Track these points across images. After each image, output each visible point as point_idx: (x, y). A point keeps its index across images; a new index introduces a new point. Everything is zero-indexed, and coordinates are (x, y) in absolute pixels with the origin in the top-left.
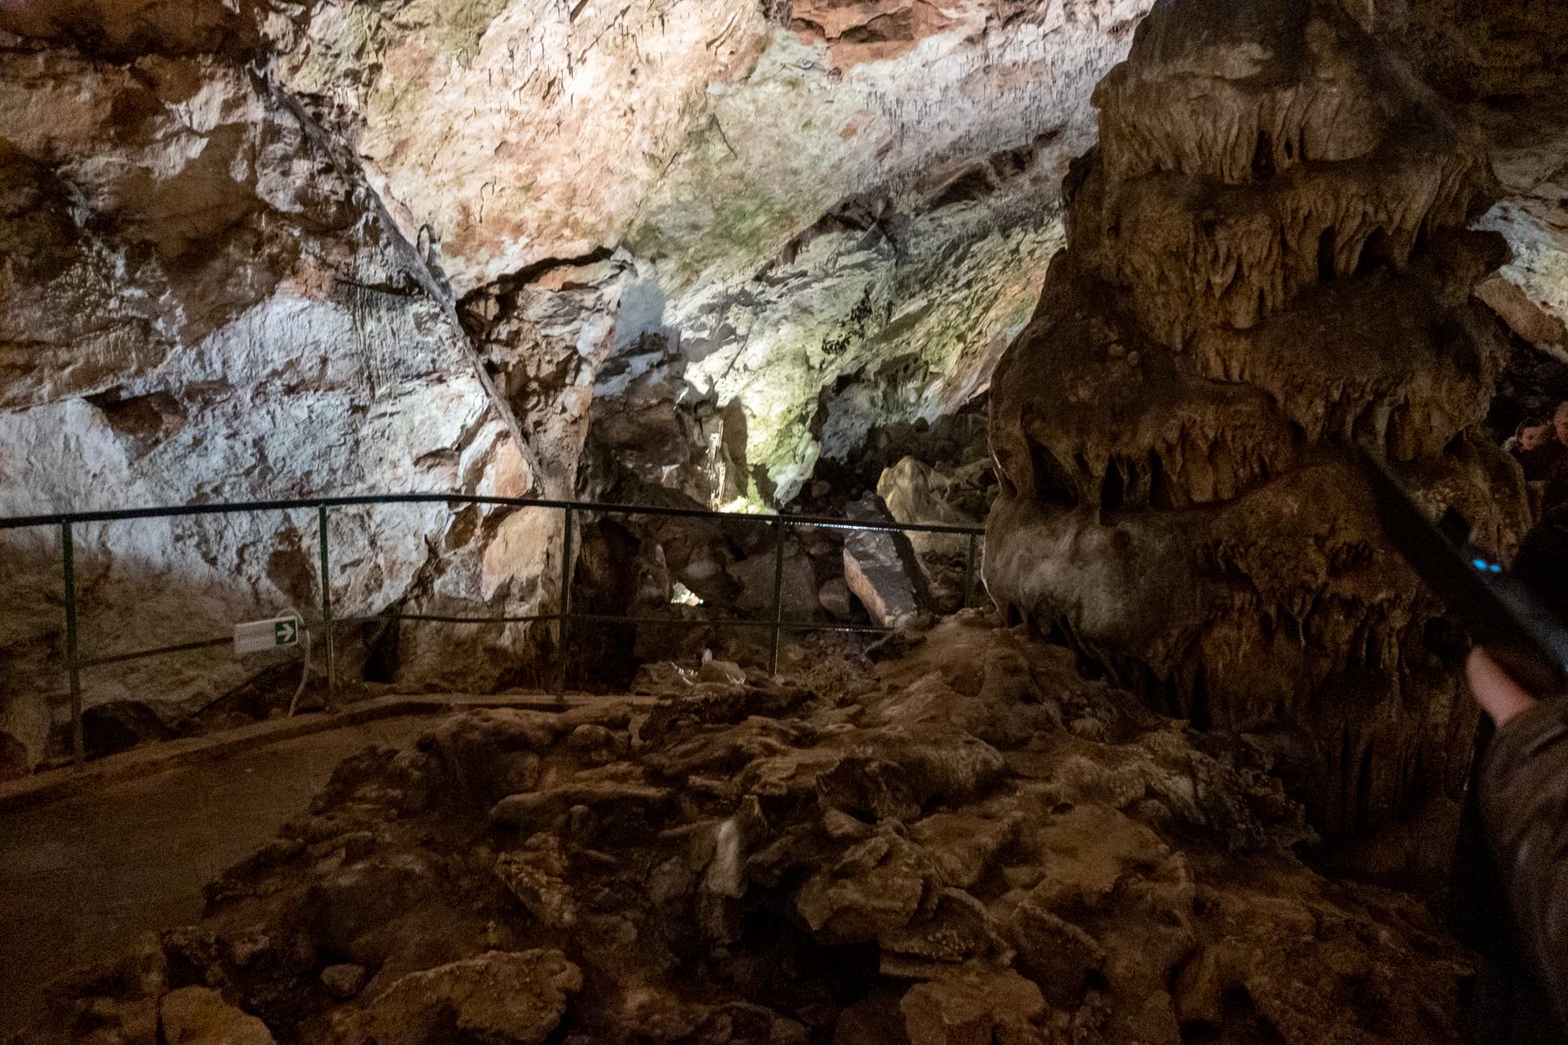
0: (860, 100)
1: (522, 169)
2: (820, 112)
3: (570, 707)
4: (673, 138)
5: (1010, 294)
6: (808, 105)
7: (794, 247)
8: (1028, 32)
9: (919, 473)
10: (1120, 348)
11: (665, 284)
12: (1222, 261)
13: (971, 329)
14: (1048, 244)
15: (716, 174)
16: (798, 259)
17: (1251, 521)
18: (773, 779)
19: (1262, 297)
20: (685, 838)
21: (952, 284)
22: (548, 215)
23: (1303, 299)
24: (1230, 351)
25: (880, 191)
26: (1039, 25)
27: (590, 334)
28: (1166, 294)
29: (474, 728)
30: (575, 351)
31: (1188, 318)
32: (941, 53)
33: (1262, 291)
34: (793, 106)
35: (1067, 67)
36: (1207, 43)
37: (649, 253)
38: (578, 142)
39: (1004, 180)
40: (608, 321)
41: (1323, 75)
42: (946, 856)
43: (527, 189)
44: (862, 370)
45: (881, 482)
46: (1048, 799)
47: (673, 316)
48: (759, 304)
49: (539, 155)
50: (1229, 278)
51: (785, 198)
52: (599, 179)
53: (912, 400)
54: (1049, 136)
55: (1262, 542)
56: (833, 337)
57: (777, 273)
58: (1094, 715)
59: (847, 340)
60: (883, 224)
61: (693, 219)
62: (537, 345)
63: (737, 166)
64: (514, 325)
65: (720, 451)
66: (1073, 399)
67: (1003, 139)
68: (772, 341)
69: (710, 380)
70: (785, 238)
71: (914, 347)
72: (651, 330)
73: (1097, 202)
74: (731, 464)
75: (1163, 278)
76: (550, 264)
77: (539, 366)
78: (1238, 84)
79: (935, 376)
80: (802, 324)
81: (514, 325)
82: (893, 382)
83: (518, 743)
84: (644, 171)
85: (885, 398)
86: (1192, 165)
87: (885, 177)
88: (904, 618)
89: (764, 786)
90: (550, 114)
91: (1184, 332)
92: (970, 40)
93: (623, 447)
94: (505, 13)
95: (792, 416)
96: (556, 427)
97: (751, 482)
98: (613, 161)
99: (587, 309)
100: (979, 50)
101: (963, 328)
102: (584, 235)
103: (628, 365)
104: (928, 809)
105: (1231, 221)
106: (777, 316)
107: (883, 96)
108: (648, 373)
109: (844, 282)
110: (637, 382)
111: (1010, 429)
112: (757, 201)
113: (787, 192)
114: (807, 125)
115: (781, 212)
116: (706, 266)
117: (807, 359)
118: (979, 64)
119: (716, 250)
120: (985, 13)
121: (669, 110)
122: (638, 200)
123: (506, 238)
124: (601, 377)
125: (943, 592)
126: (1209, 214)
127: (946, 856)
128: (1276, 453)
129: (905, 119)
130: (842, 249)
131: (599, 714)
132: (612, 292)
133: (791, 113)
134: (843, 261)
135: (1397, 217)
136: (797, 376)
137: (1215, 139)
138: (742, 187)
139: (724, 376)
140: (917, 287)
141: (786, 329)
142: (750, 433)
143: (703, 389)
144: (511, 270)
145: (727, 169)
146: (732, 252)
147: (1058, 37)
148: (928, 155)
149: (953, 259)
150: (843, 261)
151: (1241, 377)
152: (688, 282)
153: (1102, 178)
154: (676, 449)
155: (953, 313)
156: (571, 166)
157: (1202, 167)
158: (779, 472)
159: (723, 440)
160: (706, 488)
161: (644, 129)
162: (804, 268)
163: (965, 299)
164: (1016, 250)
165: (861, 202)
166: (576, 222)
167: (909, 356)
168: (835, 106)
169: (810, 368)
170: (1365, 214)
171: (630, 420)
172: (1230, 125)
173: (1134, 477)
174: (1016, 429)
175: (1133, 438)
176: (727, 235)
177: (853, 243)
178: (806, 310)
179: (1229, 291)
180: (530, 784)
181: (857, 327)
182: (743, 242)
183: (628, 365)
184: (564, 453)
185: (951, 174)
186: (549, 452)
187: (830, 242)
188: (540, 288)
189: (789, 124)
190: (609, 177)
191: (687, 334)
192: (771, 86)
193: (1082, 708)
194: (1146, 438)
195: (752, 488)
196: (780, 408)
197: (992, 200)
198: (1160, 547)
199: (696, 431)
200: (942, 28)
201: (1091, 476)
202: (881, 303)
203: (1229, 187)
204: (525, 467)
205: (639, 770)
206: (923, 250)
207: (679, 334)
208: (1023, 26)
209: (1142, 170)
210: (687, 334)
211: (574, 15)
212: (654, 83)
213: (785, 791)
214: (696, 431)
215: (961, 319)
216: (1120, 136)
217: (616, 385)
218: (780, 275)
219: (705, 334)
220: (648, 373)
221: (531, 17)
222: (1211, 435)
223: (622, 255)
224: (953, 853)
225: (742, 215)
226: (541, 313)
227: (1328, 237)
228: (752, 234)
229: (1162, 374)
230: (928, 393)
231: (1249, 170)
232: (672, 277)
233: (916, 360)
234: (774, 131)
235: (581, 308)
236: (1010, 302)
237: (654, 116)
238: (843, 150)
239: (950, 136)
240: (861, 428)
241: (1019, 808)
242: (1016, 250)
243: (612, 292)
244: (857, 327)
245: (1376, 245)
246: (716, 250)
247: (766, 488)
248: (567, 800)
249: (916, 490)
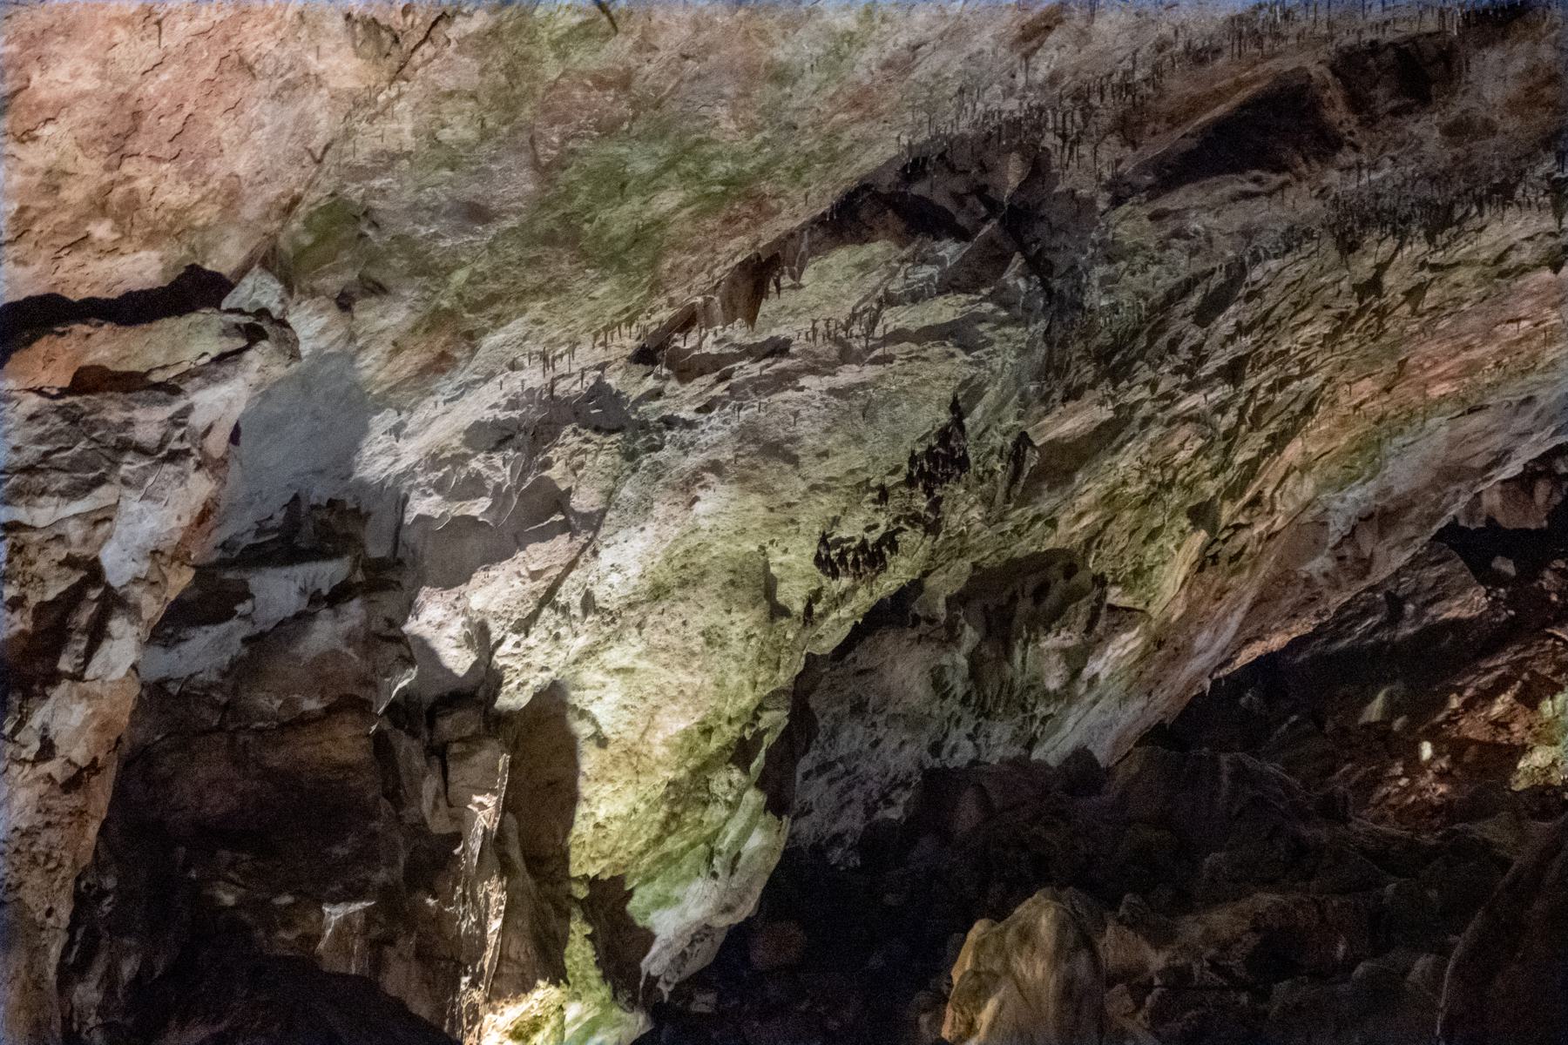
7: (758, 276)
9: (1079, 938)
11: (372, 366)
13: (1232, 492)
14: (1462, 275)
15: (551, 70)
16: (766, 307)
22: (53, 180)
25: (1018, 134)
27: (144, 526)
30: (94, 572)
37: (333, 283)
39: (1369, 122)
40: (201, 487)
45: (965, 962)
47: (384, 455)
48: (644, 426)
52: (212, 87)
53: (1053, 684)
56: (852, 529)
57: (704, 342)
59: (890, 540)
61: (473, 191)
63: (618, 50)
65: (496, 842)
68: (672, 532)
69: (480, 637)
70: (737, 248)
71: (1068, 533)
72: (320, 492)
74: (526, 880)
79: (1124, 617)
84: (343, 67)
85: (975, 674)
87: (1034, 99)
93: (211, 836)
95: (715, 744)
97: (579, 929)
98: (258, 41)
99: (142, 451)
101: (1210, 488)
102: (151, 240)
103: (245, 595)
106: (693, 461)
108: (302, 619)
109: (894, 378)
113: (753, 129)
115: (728, 182)
116: (499, 321)
117: (769, 587)
119: (533, 278)
122: (317, 143)
124: (165, 633)
130: (896, 286)
132: (218, 403)
134: (894, 318)
136: (736, 631)
138: (624, 108)
140: (1089, 372)
141: (713, 501)
142: (585, 789)
143: (458, 660)
145: (585, 59)
148: (1161, 47)
149: (1194, 300)
150: (894, 318)
152: (442, 363)
154: (368, 856)
155: (1185, 445)
156: (133, 51)
158: (662, 902)
159: (507, 807)
162: (781, 332)
163: (1222, 409)
164: (1373, 286)
165: (962, 159)
166: (133, 203)
167: (1053, 553)
169: (778, 611)
176: (565, 237)
177: (927, 270)
178: (780, 451)
181: (921, 503)
182: (608, 259)
183: (245, 595)
185: (1219, 96)
195: (579, 952)
196: (676, 723)
197: (1333, 176)
199: (430, 786)
202: (997, 440)
206: (1125, 297)
210: (424, 505)
215: (1206, 465)
217: (204, 652)
218: (709, 347)
219: (478, 508)
220: (302, 619)
223: (261, 291)
225: (615, 183)
228: (639, 237)
230: (1098, 666)
232: (397, 348)
233: (1070, 571)
235: (125, 446)
236: (1344, 422)
240: (902, 754)
242: (1373, 286)
243: (218, 403)
246: (533, 278)
249: (1068, 992)
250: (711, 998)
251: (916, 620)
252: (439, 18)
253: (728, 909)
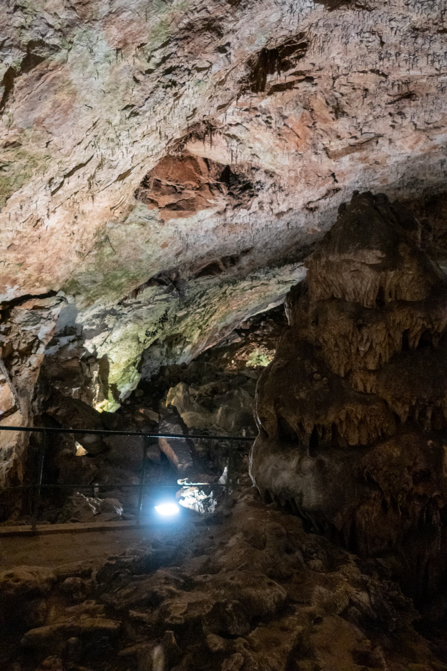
0: (171, 233)
1: (19, 256)
2: (154, 237)
3: (40, 533)
4: (89, 245)
5: (221, 310)
6: (148, 234)
7: (137, 292)
8: (243, 212)
9: (186, 389)
10: (319, 376)
11: (78, 306)
12: (364, 341)
13: (204, 324)
15: (106, 260)
16: (138, 296)
17: (380, 459)
18: (177, 614)
19: (380, 357)
20: (134, 655)
21: (198, 305)
22: (30, 276)
23: (395, 358)
24: (367, 380)
25: (175, 270)
27: (45, 330)
28: (338, 352)
29: (10, 586)
30: (37, 337)
31: (347, 363)
32: (206, 217)
33: (380, 354)
34: (142, 234)
35: (258, 227)
36: (359, 248)
37: (72, 293)
38: (47, 246)
39: (226, 268)
40: (53, 324)
41: (406, 266)
42: (269, 658)
43: (20, 265)
46: (311, 616)
47: (80, 319)
48: (119, 314)
49: (28, 250)
50: (367, 348)
51: (135, 271)
53: (178, 353)
54: (246, 252)
55: (385, 469)
56: (151, 330)
57: (128, 302)
58: (318, 558)
60: (175, 283)
61: (94, 278)
62: (19, 334)
63: (116, 257)
64: (8, 325)
65: (97, 379)
66: (297, 397)
67: (228, 251)
68: (124, 330)
69: (94, 347)
70: (133, 287)
71: (180, 330)
72: (70, 325)
73: (306, 309)
74: (102, 384)
75: (336, 345)
76: (28, 297)
77: (19, 345)
78: (372, 266)
79: (189, 343)
80: (138, 324)
81: (8, 325)
82: (171, 345)
83: (31, 593)
84: (75, 259)
86: (350, 298)
88: (187, 465)
89: (172, 619)
90: (36, 234)
91: (345, 369)
92: (219, 213)
93: (55, 379)
94: (21, 190)
95: (130, 363)
96: (25, 373)
98: (62, 255)
99: (44, 318)
100: (222, 217)
101: (201, 323)
102: (45, 286)
103: (58, 341)
104: (253, 626)
105: (369, 325)
107: (181, 232)
109: (157, 306)
110: (62, 349)
111: (268, 409)
112: (123, 272)
114: (148, 242)
115: (133, 277)
116: (98, 298)
117: (138, 338)
118: (223, 222)
119: (103, 292)
120: (226, 203)
121: (89, 233)
122: (71, 271)
123: (8, 286)
125: (200, 449)
126: (360, 321)
127: (269, 658)
128: (388, 428)
129: (189, 242)
131: (76, 569)
132: (56, 311)
133: (141, 236)
134: (157, 298)
135: (436, 327)
136: (133, 346)
137: (361, 289)
138: (117, 266)
139: (101, 345)
140: (183, 306)
141: (130, 326)
142: (110, 370)
143: (91, 351)
144: (8, 300)
146: (110, 293)
147: (255, 215)
148: (196, 257)
150: (157, 298)
151: (371, 391)
152: (89, 305)
153: (308, 298)
154: (79, 380)
155: (197, 317)
156: (43, 256)
157: (355, 299)
158: (122, 387)
160: (91, 396)
161: (77, 241)
162: (140, 300)
164: (225, 293)
165: (167, 274)
166: (42, 280)
167: (177, 335)
168: (160, 235)
169: (140, 342)
170: (423, 325)
171: (58, 366)
172: (368, 283)
173: (324, 433)
174: (271, 410)
175: (326, 418)
176: (108, 285)
178: (140, 318)
179: (366, 354)
180: (41, 620)
182: (115, 289)
183: (58, 341)
184: (28, 385)
186: (21, 385)
187: (153, 290)
188: (22, 308)
189: (139, 241)
190: (60, 261)
191: (86, 327)
192: (133, 225)
193: (312, 554)
194: (331, 418)
195: (110, 395)
196: (125, 359)
198: (338, 468)
199: (87, 370)
200: (207, 207)
201: (305, 432)
202: (172, 316)
203: (367, 309)
204: (12, 395)
205: (102, 606)
207: (82, 327)
208: (241, 210)
209: (326, 297)
210: (86, 327)
211: (53, 193)
212: (84, 222)
213: (183, 621)
214: (87, 370)
216: (317, 281)
218: (129, 302)
219: (94, 327)
220: (68, 345)
221: (33, 192)
222: (359, 417)
223: (61, 294)
224: (273, 657)
225: (115, 277)
226: (22, 320)
227: (406, 333)
228: (119, 286)
229: (337, 389)
230: (185, 350)
231: (374, 302)
232: (82, 303)
233: (181, 336)
234: (133, 244)
235: (41, 318)
237: (83, 235)
238: (161, 253)
239: (206, 250)
240: (156, 364)
241: (298, 623)
242: (225, 293)
243: (56, 311)
244: (161, 325)
245: (426, 337)
246: (103, 292)
247: (116, 394)
248: (66, 632)
249: (185, 397)
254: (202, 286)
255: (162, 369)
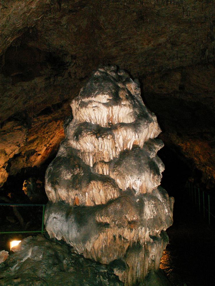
8: (59, 78)
16: (3, 127)
26: (63, 77)
44: (21, 153)
250: (3, 189)
251: (21, 156)
252: (96, 106)
253: (4, 181)
254: (41, 121)
255: (23, 169)
